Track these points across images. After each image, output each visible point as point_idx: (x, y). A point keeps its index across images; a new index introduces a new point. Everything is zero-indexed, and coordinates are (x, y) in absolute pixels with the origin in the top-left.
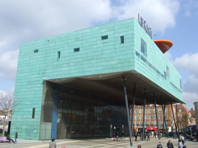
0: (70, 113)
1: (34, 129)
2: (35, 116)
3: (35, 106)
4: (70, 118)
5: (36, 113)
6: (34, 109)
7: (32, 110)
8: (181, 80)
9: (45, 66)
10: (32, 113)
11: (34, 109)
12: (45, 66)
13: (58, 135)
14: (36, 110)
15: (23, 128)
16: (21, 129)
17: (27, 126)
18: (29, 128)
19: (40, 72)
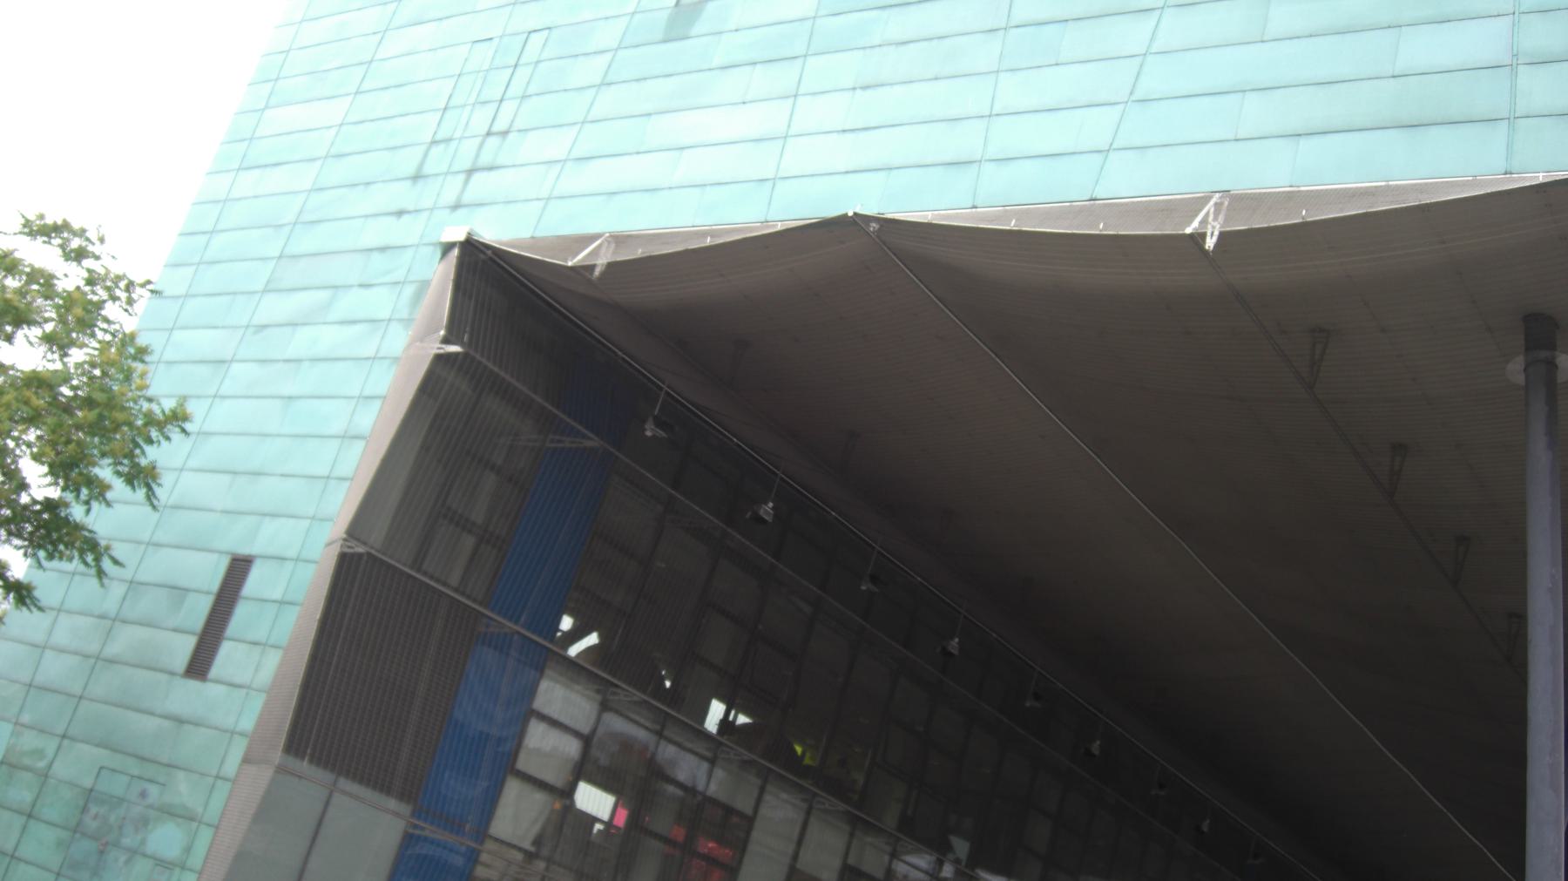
0: (663, 743)
1: (170, 812)
2: (228, 657)
3: (259, 540)
4: (667, 841)
5: (241, 614)
6: (239, 567)
7: (211, 573)
8: (1229, 191)
9: (516, 89)
10: (201, 608)
11: (239, 567)
12: (516, 89)
13: (95, 520)
14: (255, 583)
15: (61, 770)
16: (45, 775)
17: (104, 757)
18: (117, 785)
19: (438, 161)
